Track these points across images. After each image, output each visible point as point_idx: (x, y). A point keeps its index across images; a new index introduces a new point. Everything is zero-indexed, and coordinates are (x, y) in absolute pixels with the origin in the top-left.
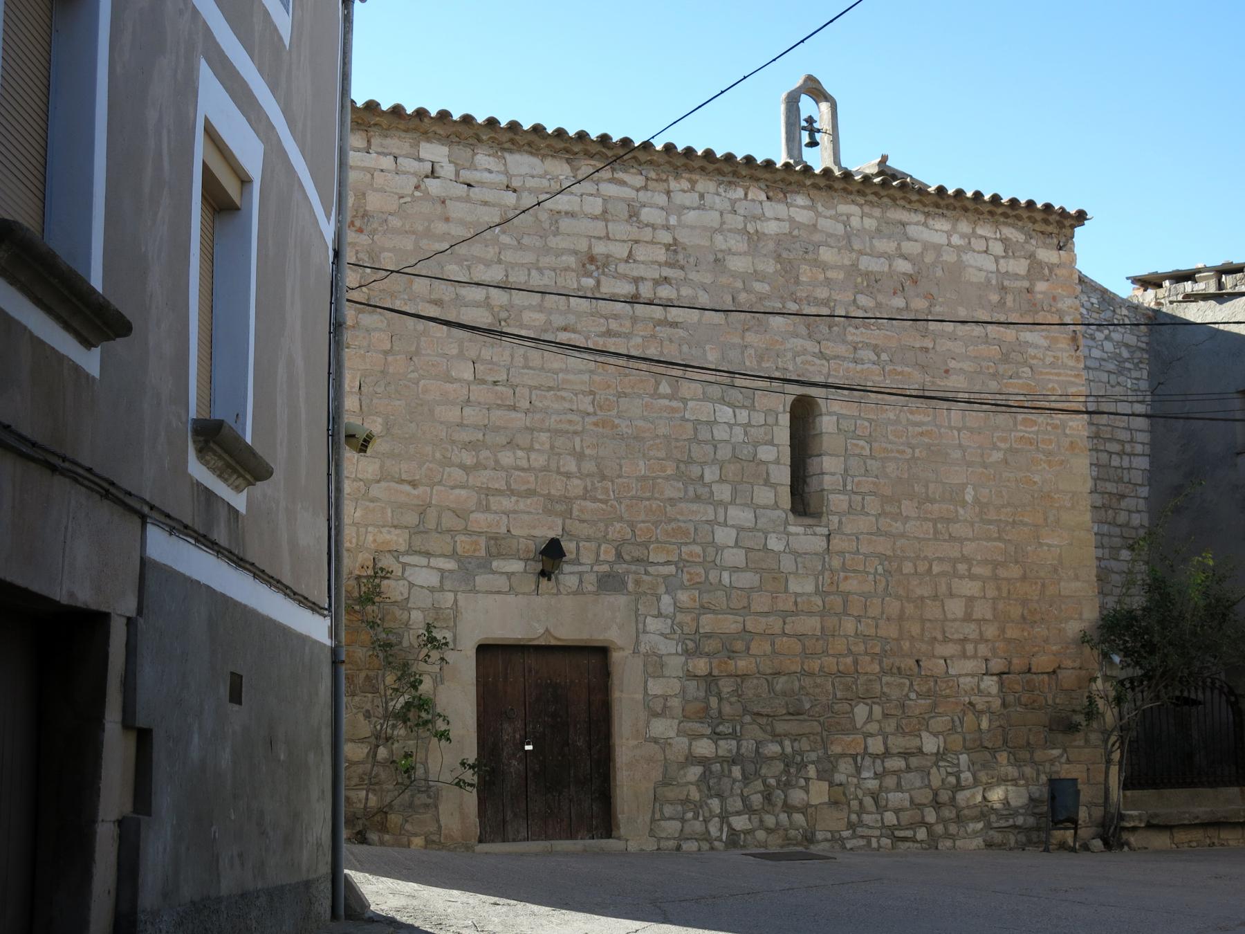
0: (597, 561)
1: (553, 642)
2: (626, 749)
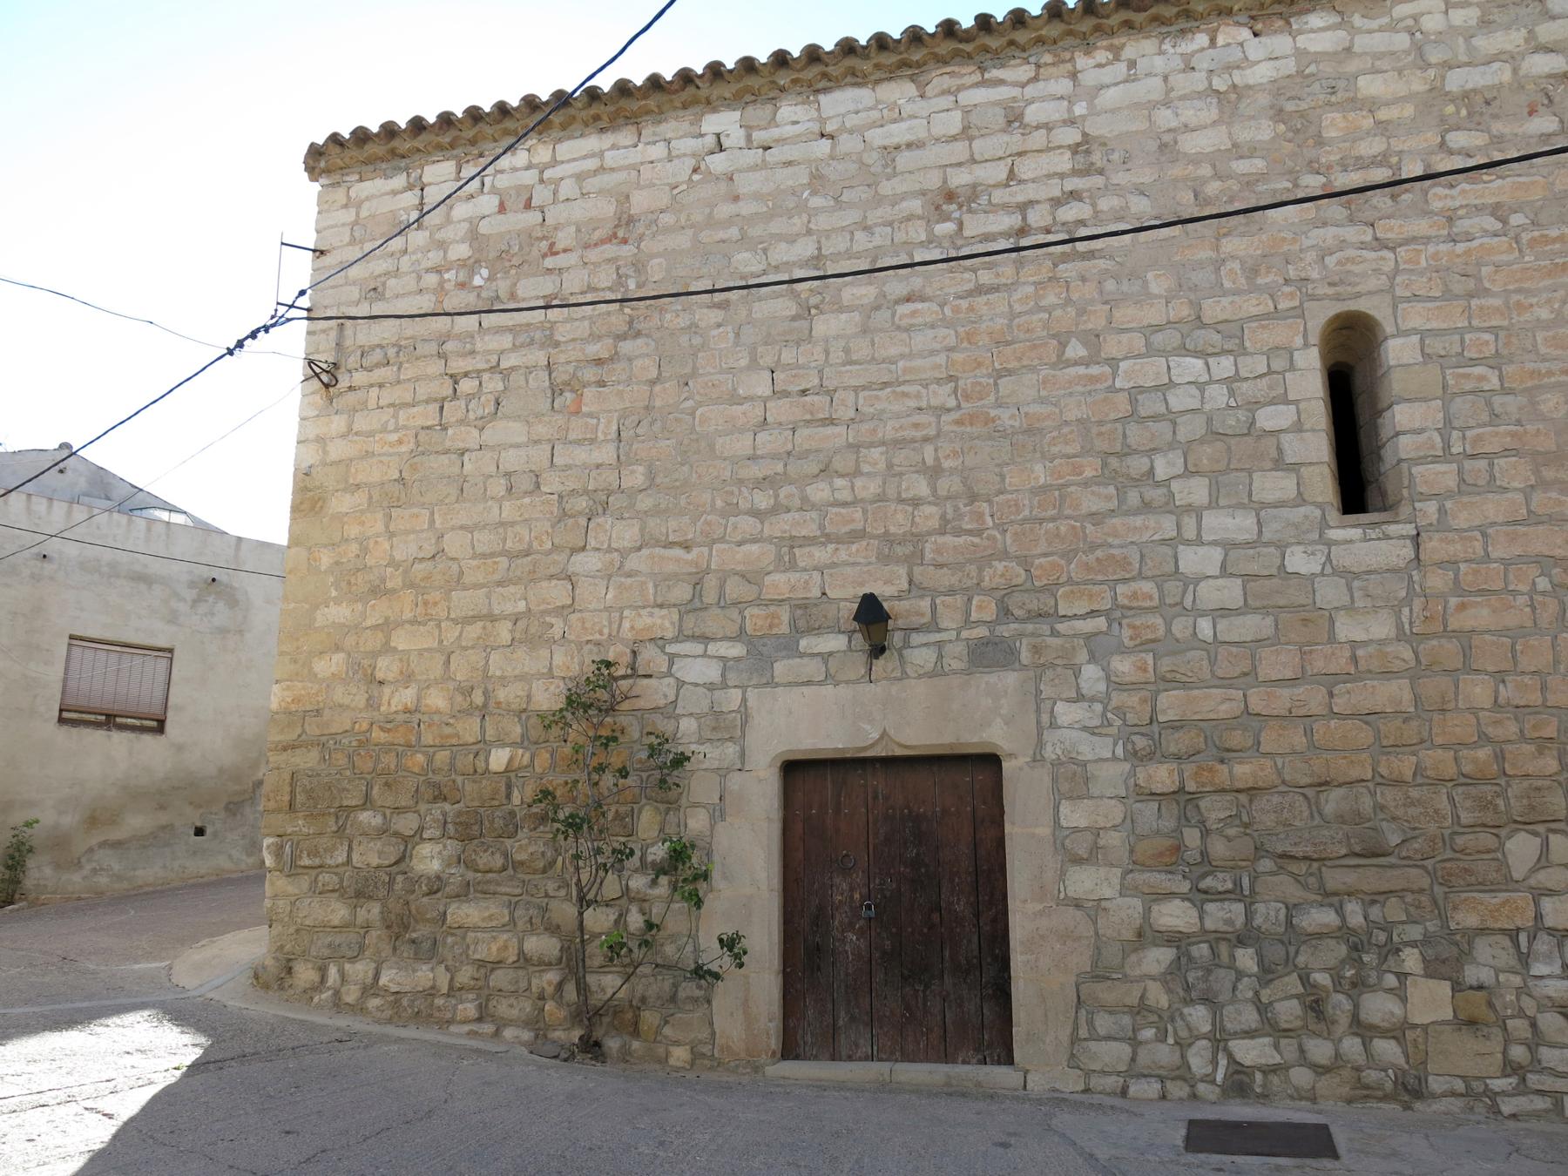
0: (968, 623)
1: (899, 752)
2: (1025, 918)
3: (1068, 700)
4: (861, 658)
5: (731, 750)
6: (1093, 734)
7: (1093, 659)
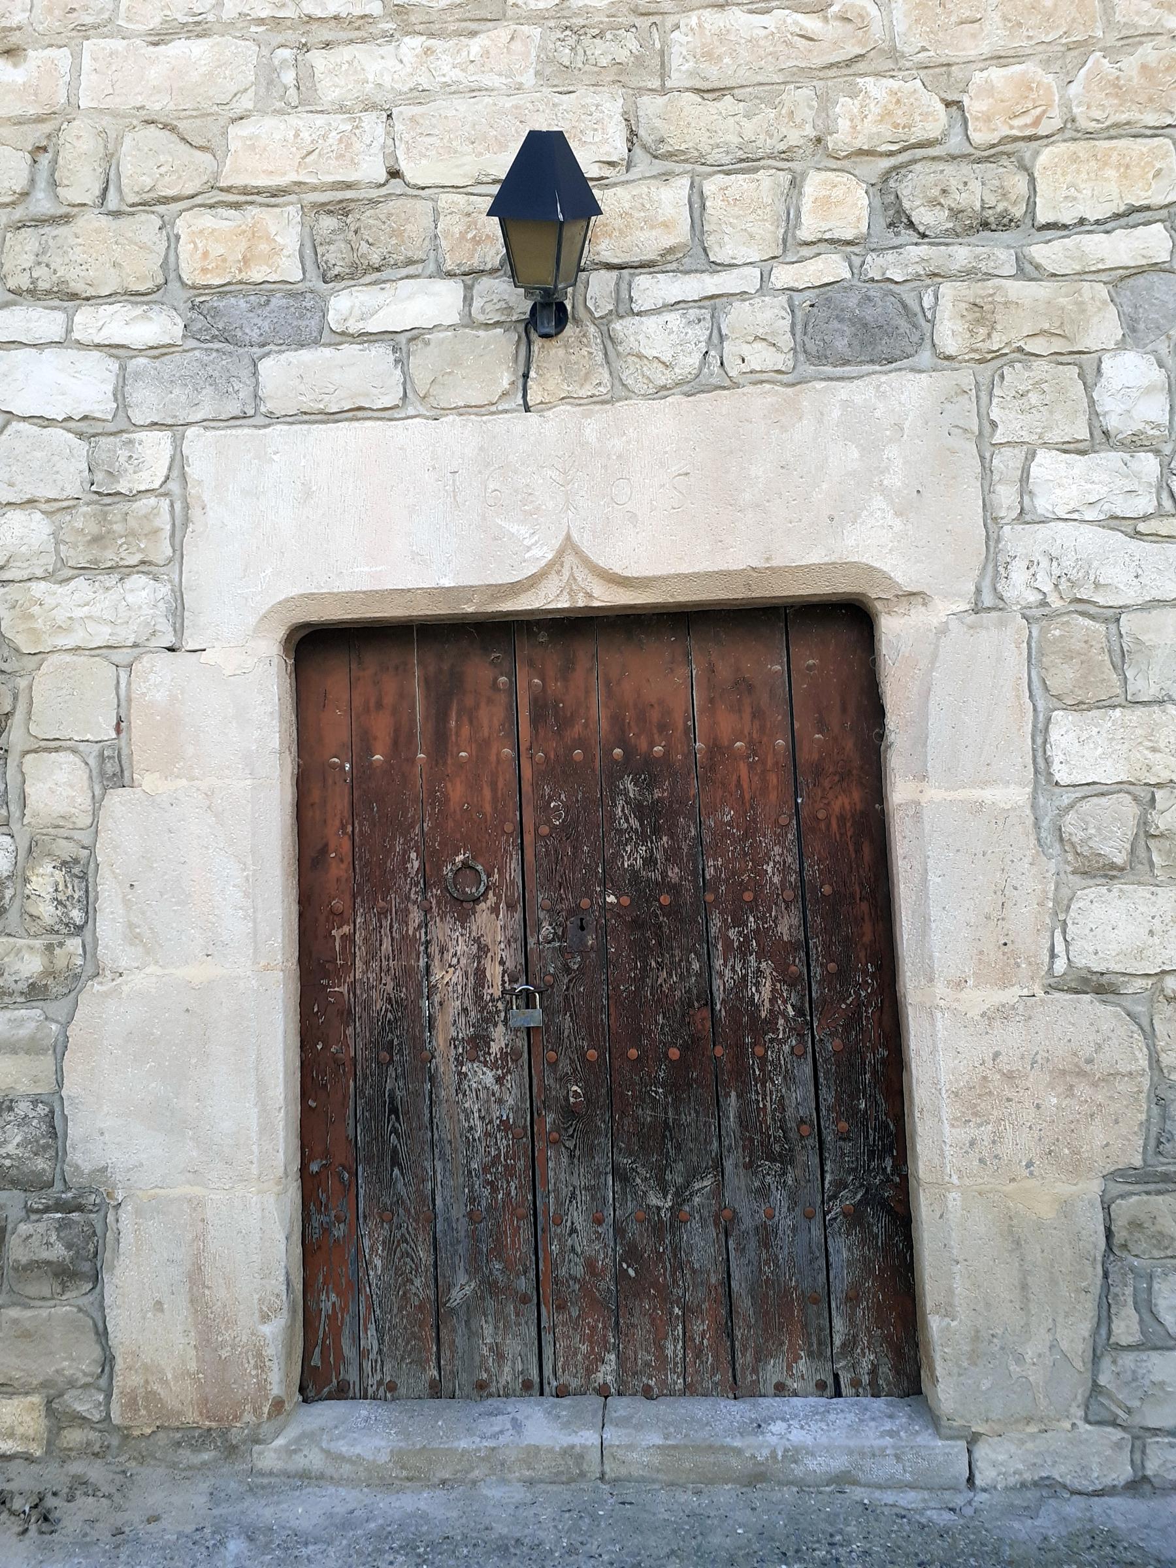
0: (791, 245)
1: (604, 597)
2: (963, 1022)
3: (1069, 448)
4: (501, 345)
5: (142, 593)
6: (1137, 535)
7: (1133, 334)
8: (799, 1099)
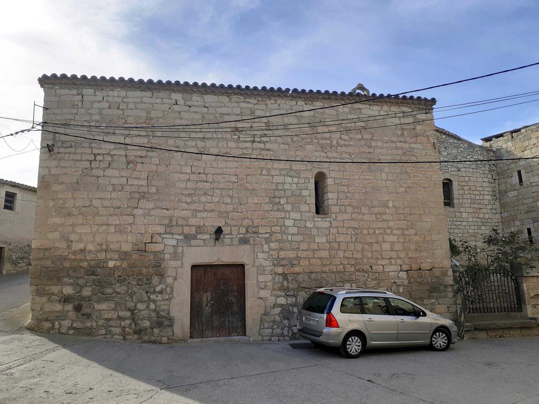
0: (239, 234)
1: (221, 263)
5: (179, 262)
8: (236, 310)
